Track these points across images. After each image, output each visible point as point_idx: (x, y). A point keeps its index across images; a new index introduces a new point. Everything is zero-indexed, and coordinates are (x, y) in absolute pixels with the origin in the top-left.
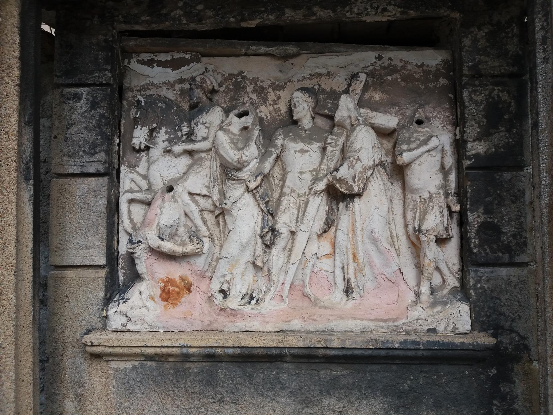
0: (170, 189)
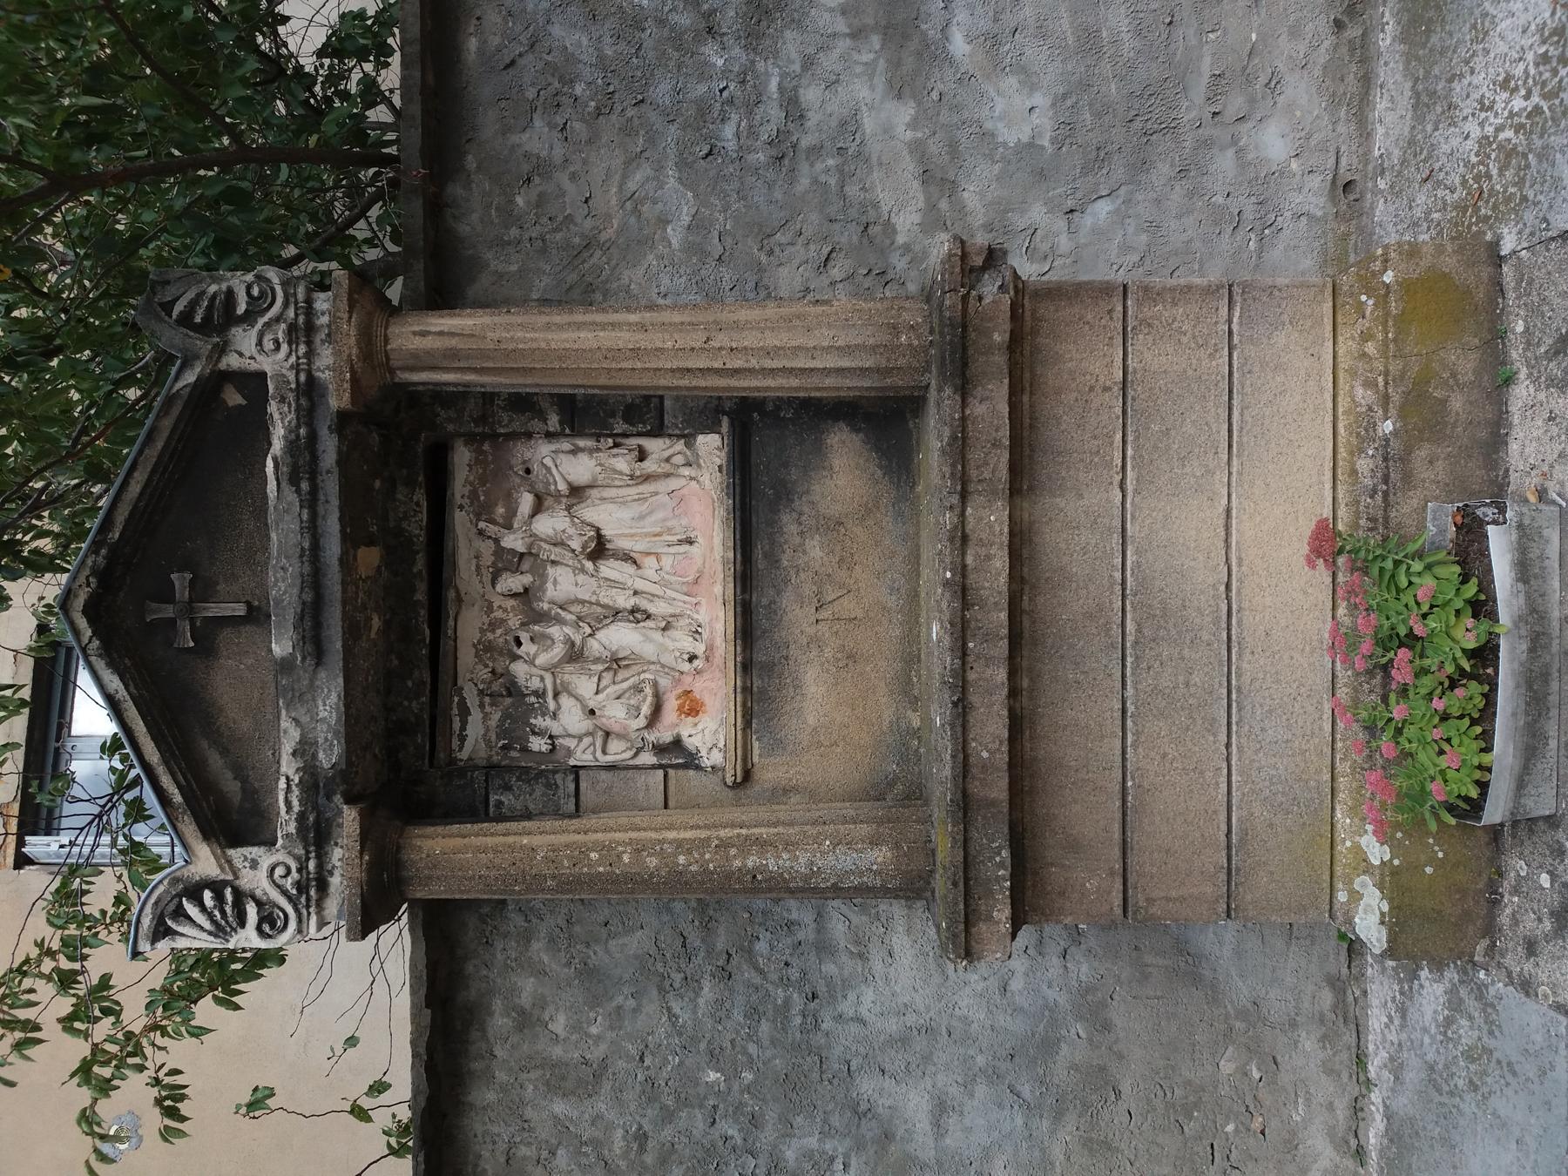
0: (592, 712)
